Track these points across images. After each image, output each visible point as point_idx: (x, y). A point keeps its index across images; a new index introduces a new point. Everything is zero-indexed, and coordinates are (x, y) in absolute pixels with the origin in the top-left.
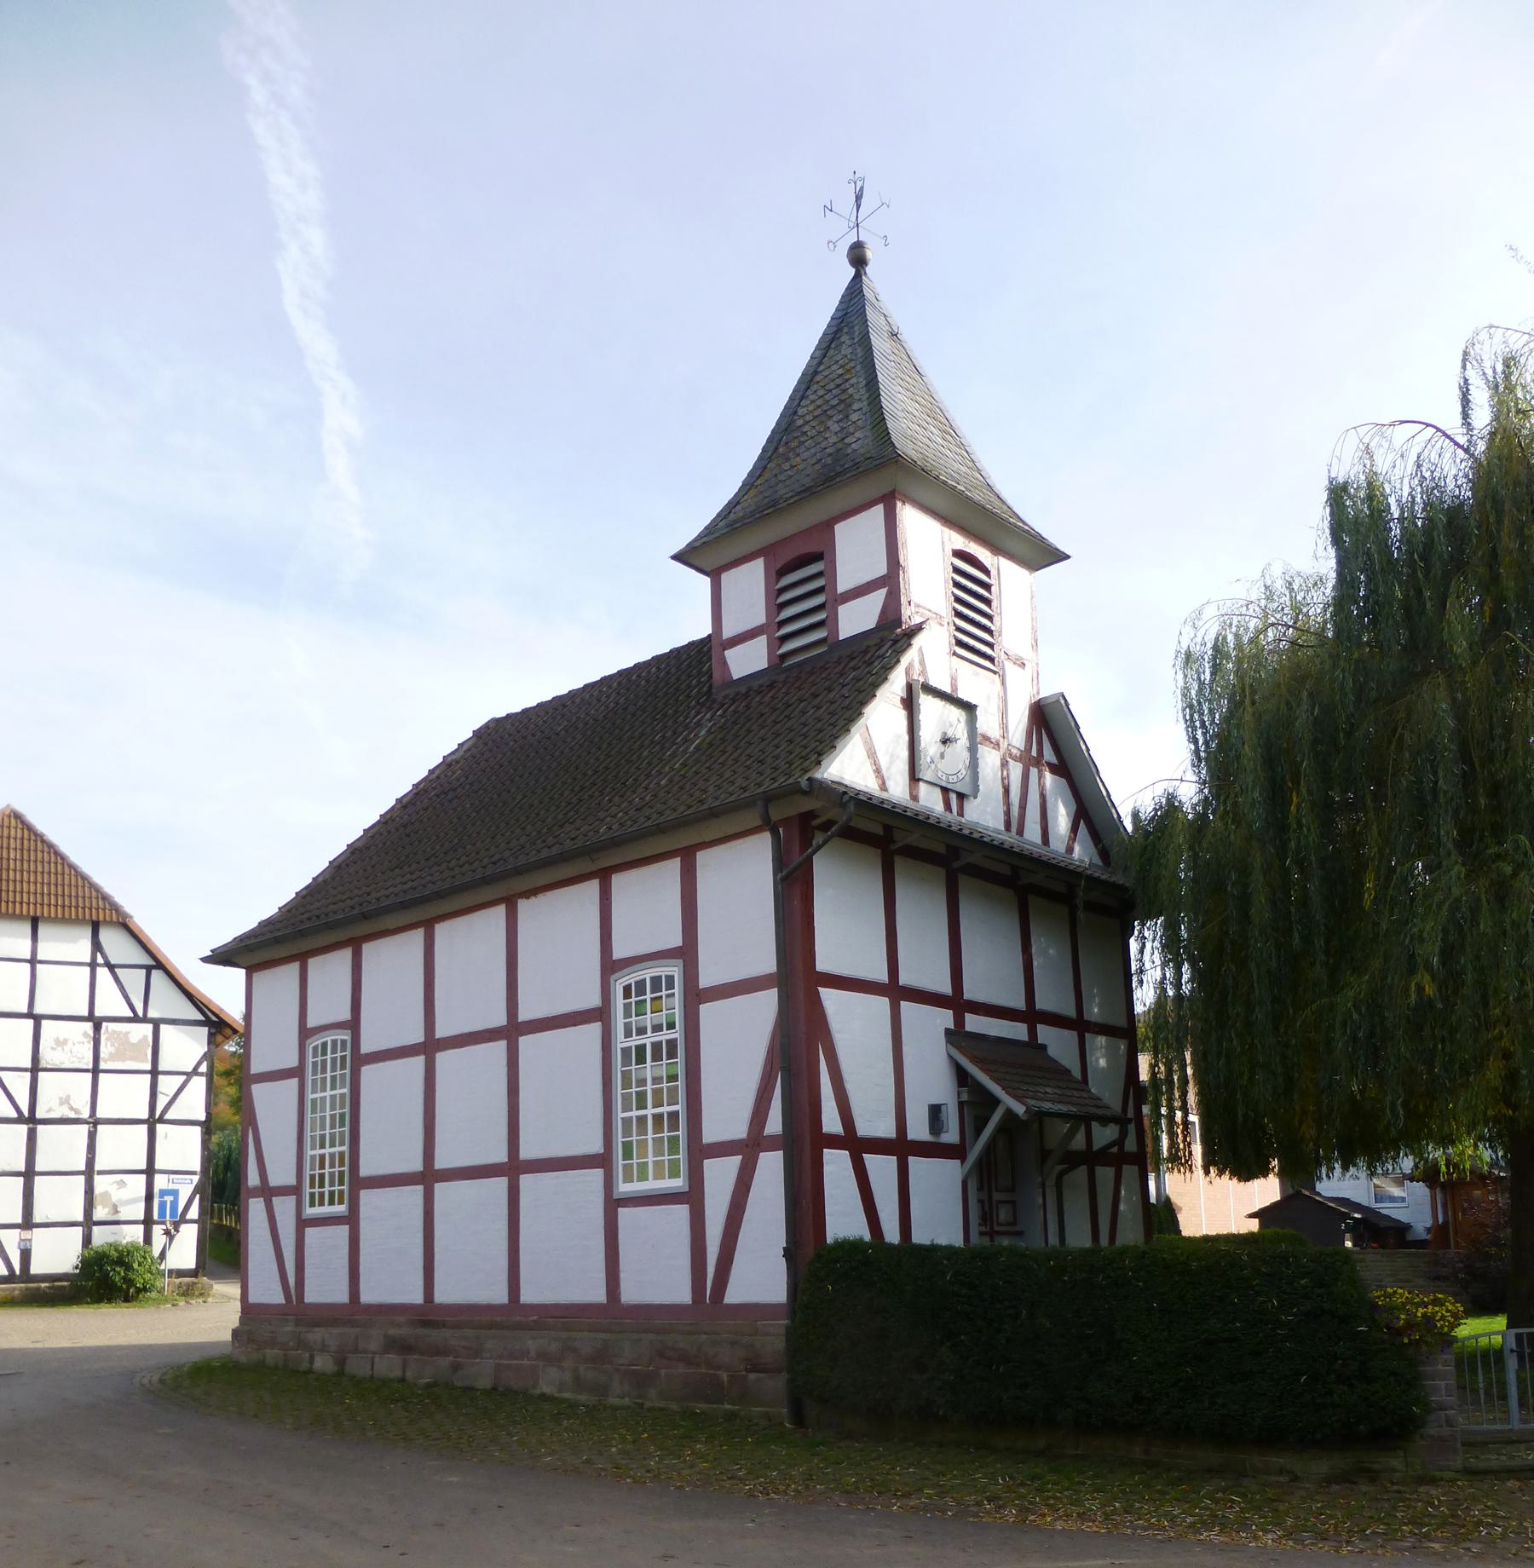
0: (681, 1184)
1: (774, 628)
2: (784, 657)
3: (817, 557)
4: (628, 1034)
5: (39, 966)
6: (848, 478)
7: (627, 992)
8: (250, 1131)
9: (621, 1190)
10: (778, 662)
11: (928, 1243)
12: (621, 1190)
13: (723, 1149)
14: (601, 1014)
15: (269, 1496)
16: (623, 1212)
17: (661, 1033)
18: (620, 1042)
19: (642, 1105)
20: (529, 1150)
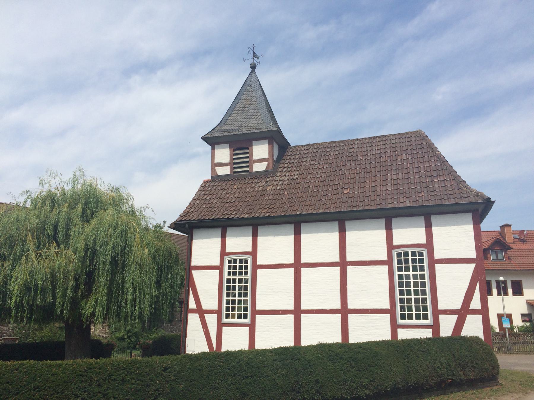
0: (248, 321)
1: (232, 164)
2: (235, 172)
3: (248, 149)
4: (229, 274)
5: (337, 259)
6: (248, 129)
7: (230, 262)
8: (190, 289)
9: (224, 321)
10: (233, 173)
11: (420, 338)
12: (224, 321)
13: (475, 312)
14: (220, 268)
15: (397, 366)
16: (224, 329)
17: (236, 276)
18: (226, 276)
19: (240, 295)
20: (337, 305)
